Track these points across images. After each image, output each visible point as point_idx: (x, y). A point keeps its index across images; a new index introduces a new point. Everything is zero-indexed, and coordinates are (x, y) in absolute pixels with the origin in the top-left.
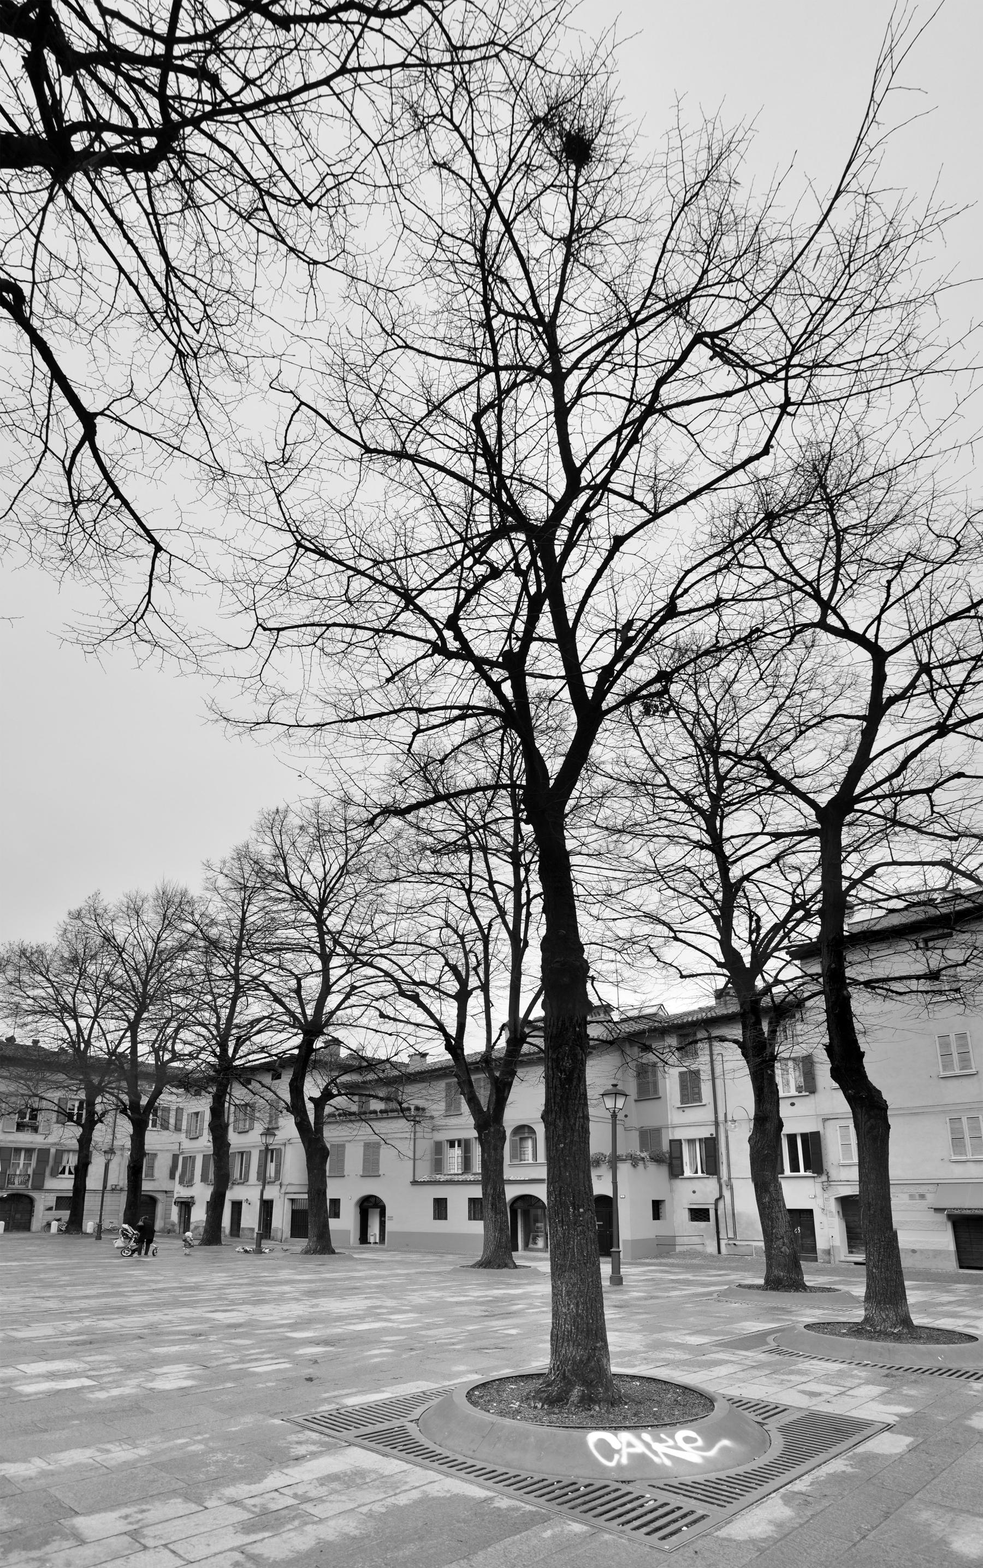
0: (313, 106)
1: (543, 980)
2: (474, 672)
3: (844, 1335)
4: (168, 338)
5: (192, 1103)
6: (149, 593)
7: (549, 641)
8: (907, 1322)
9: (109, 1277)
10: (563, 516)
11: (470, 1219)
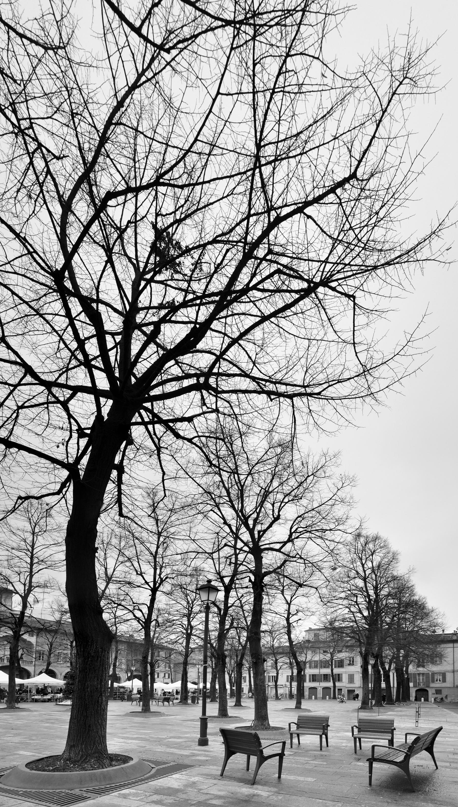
2: (284, 627)
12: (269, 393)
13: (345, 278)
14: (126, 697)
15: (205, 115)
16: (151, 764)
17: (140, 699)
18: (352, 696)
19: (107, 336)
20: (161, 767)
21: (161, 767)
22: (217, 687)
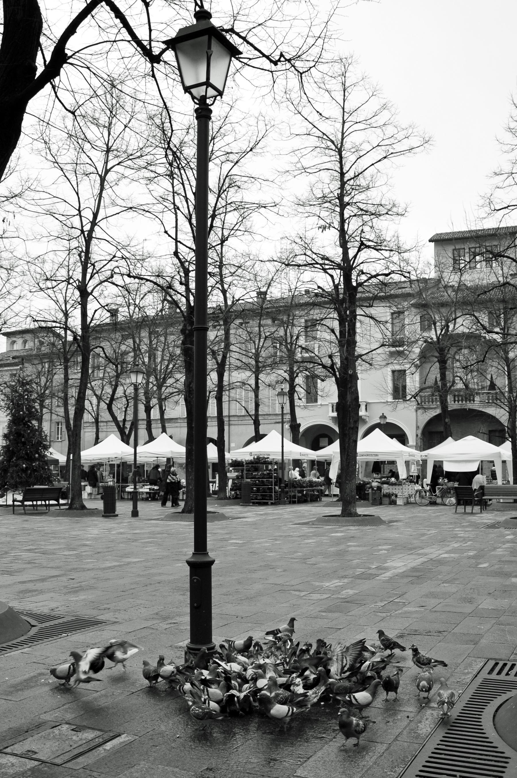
0: (106, 71)
1: (62, 67)
2: (70, 367)
3: (427, 505)
4: (244, 39)
5: (367, 758)
6: (77, 194)
7: (54, 87)
8: (83, 507)
9: (36, 549)
10: (197, 271)
11: (435, 461)
12: (130, 159)
13: (59, 549)
14: (309, 499)
15: (76, 752)
16: (29, 619)
17: (131, 499)
18: (387, 469)
19: (49, 83)
20: (47, 624)
21: (47, 624)
22: (71, 458)
